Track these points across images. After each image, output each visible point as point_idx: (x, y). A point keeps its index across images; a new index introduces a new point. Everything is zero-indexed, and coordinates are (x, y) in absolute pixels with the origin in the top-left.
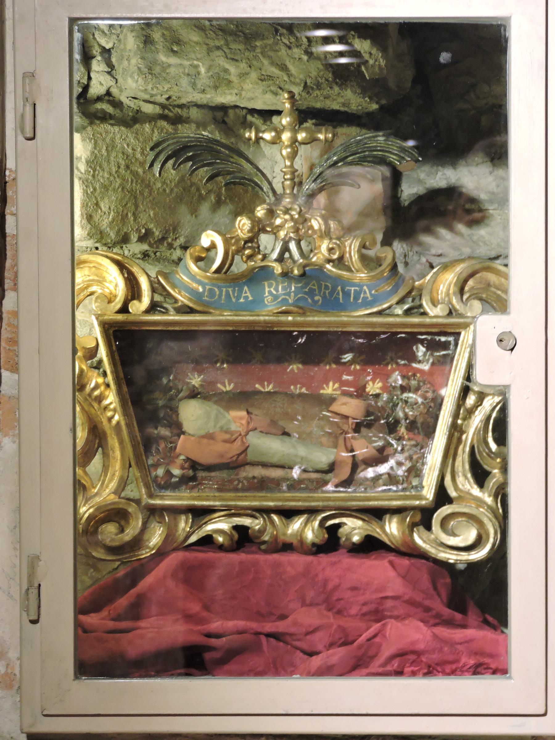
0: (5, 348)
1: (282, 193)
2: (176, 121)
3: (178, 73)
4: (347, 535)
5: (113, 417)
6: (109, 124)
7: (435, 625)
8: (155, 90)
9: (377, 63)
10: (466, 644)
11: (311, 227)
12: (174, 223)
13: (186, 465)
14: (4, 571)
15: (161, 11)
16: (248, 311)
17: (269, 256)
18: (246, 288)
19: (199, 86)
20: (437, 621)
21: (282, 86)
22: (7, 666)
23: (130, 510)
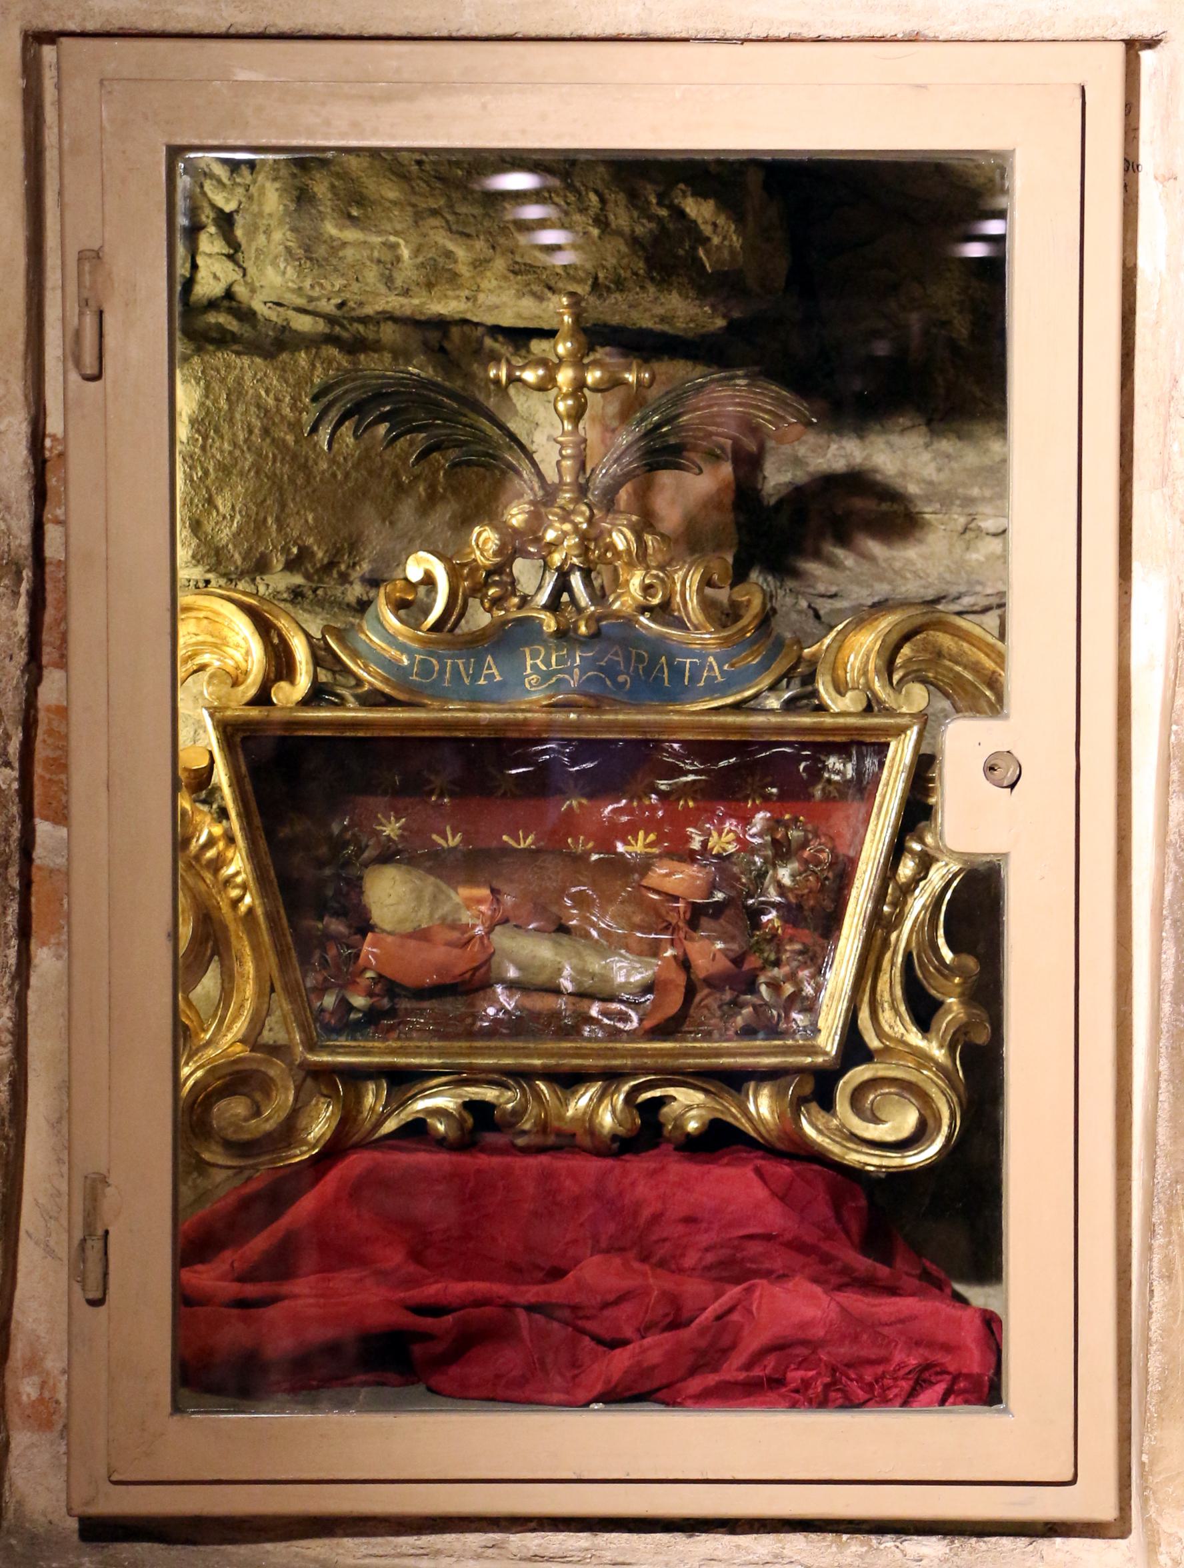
0: (42, 777)
1: (556, 480)
2: (356, 346)
3: (358, 257)
4: (676, 1119)
5: (241, 899)
6: (233, 352)
7: (840, 1288)
8: (317, 289)
9: (726, 243)
10: (900, 1326)
11: (612, 547)
12: (351, 536)
13: (378, 989)
14: (37, 1204)
15: (343, 136)
16: (493, 702)
17: (532, 600)
18: (489, 658)
19: (399, 283)
20: (846, 1280)
21: (552, 283)
22: (43, 1385)
23: (272, 1073)
